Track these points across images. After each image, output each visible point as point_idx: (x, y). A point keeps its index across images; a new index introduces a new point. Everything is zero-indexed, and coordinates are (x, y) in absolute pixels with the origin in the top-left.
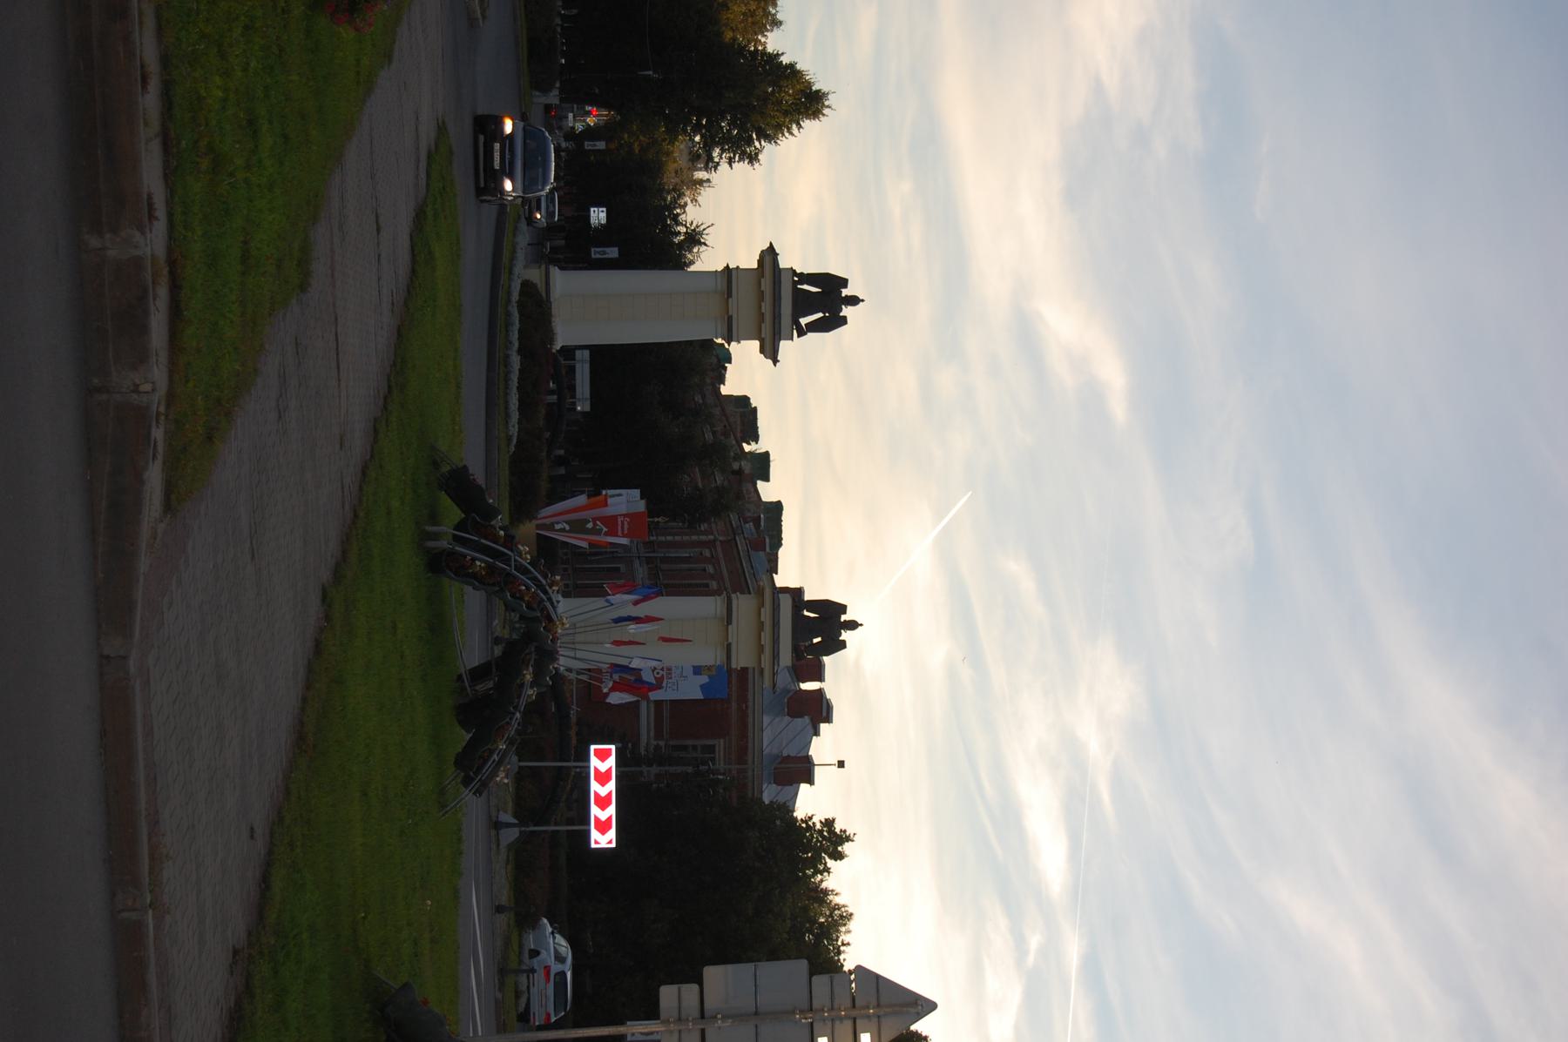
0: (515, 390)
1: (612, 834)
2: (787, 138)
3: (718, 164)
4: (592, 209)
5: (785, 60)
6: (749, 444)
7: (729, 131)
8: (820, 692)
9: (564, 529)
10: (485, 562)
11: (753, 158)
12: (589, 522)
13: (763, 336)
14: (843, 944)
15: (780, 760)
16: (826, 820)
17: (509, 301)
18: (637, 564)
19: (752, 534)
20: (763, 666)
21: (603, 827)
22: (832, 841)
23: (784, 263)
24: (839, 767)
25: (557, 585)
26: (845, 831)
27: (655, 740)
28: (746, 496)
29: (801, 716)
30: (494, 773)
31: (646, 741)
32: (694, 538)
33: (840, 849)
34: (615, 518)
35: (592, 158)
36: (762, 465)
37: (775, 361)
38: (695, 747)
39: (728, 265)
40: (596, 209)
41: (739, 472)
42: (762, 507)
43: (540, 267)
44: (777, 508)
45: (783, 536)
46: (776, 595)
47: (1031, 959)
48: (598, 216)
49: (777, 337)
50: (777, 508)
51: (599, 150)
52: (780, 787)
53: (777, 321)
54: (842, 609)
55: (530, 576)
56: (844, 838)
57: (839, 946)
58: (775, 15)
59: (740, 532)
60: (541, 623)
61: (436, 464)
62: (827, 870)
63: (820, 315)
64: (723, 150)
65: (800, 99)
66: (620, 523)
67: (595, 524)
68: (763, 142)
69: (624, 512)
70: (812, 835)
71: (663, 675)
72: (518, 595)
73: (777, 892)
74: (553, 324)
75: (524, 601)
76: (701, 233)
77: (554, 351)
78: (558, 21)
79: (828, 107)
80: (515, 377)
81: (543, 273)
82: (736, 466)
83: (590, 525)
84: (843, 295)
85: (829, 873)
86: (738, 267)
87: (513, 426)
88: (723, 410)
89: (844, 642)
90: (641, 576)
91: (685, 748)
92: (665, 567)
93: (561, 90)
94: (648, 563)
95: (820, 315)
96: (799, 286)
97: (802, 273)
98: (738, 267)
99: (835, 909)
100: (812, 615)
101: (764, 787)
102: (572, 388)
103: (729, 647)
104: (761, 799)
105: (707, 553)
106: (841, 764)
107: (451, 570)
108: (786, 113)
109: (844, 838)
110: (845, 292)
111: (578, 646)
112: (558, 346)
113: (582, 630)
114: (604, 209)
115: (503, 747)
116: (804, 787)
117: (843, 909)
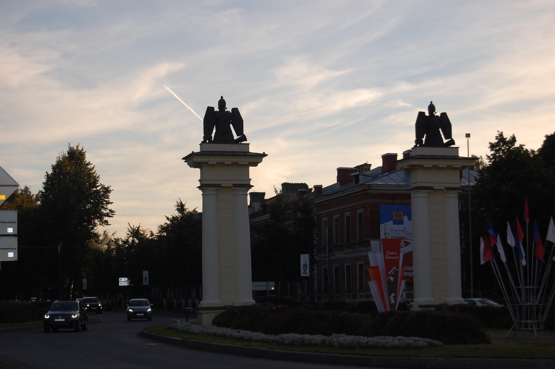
2: (95, 171)
3: (110, 210)
4: (120, 285)
5: (50, 172)
7: (91, 203)
9: (393, 296)
11: (107, 191)
12: (389, 279)
13: (247, 163)
23: (197, 149)
24: (469, 137)
34: (386, 261)
37: (264, 155)
39: (198, 187)
40: (120, 283)
42: (285, 194)
43: (200, 314)
47: (409, 105)
48: (123, 282)
51: (87, 282)
56: (501, 138)
58: (22, 190)
59: (312, 201)
65: (74, 163)
66: (390, 258)
67: (391, 275)
68: (97, 185)
71: (404, 242)
76: (133, 229)
78: (275, 296)
79: (77, 147)
80: (364, 339)
83: (392, 279)
86: (199, 180)
90: (342, 255)
97: (204, 138)
103: (448, 189)
106: (468, 135)
109: (501, 138)
110: (217, 109)
114: (120, 279)
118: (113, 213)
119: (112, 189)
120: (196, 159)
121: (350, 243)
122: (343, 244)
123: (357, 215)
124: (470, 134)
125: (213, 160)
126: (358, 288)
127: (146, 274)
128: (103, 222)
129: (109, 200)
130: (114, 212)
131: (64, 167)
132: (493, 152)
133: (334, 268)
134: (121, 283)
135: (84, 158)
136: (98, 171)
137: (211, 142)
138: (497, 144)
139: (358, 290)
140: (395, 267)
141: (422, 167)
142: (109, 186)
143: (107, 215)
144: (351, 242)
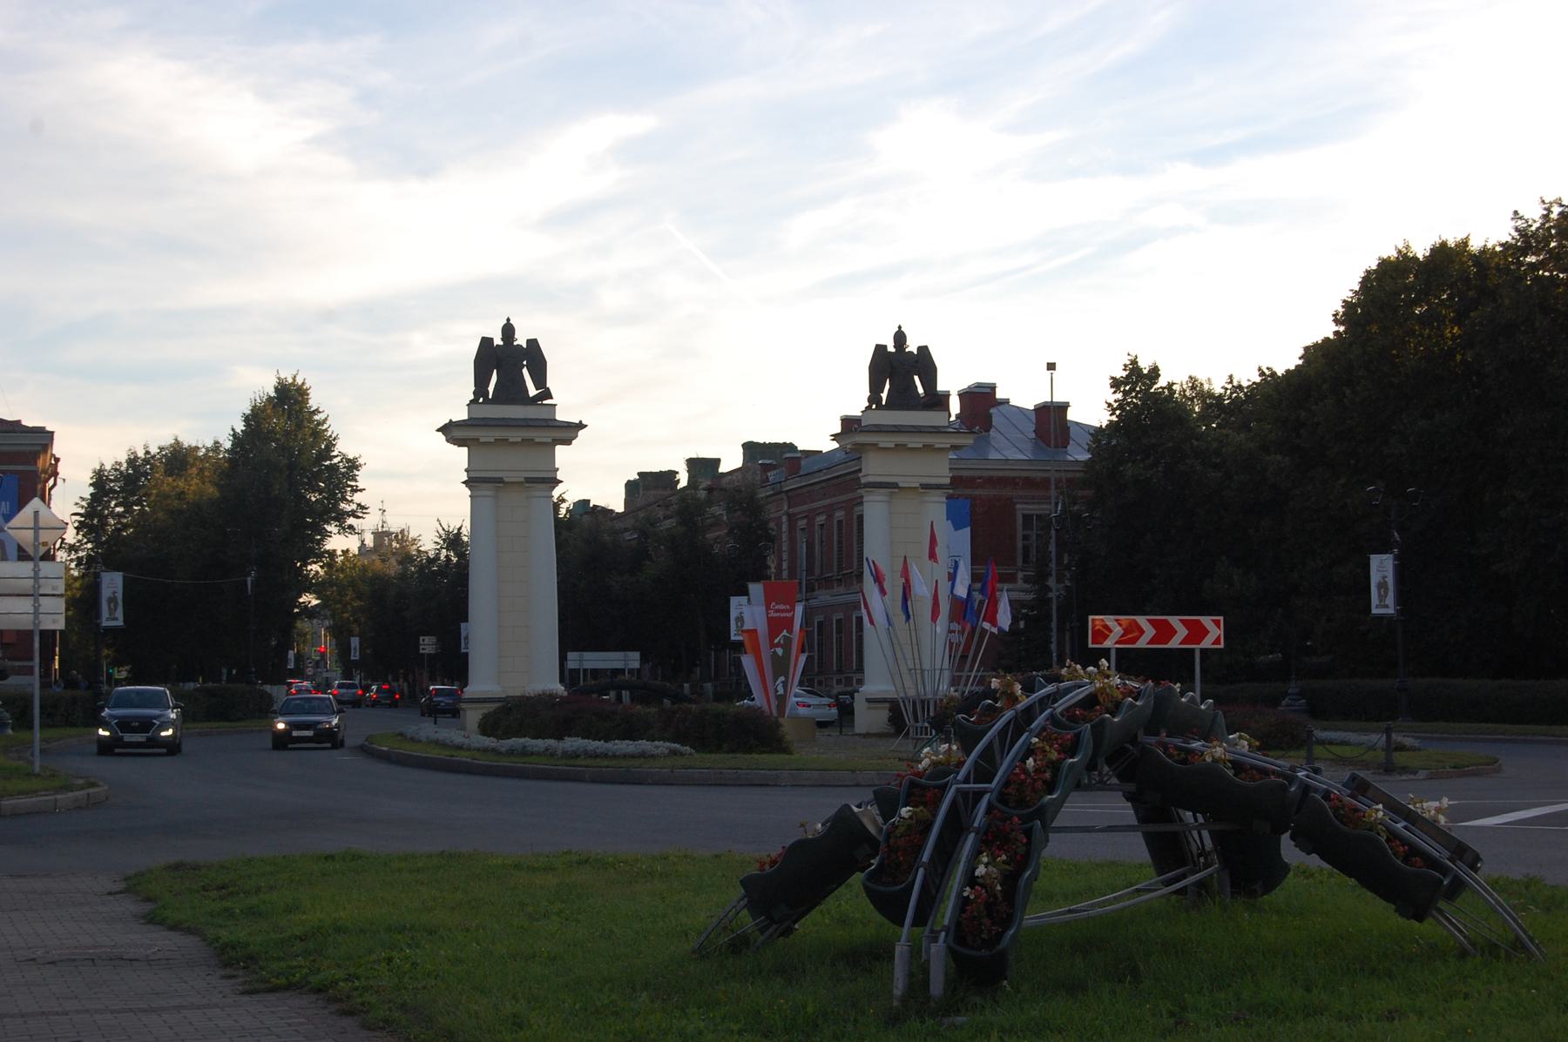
0: (609, 745)
1: (1206, 621)
3: (359, 505)
4: (421, 651)
5: (240, 427)
6: (678, 481)
8: (962, 395)
9: (783, 682)
10: (977, 853)
11: (353, 465)
12: (775, 652)
14: (1231, 382)
15: (1040, 442)
16: (1112, 387)
17: (495, 751)
18: (813, 602)
19: (782, 472)
20: (949, 446)
21: (1197, 632)
22: (1136, 380)
23: (462, 414)
24: (1054, 369)
25: (1010, 685)
26: (1125, 366)
27: (1016, 582)
28: (736, 484)
29: (990, 416)
30: (1430, 827)
31: (1017, 593)
32: (784, 537)
33: (1145, 372)
34: (771, 621)
35: (368, 651)
36: (702, 467)
37: (581, 426)
38: (1025, 538)
40: (421, 647)
41: (710, 490)
42: (749, 464)
43: (463, 709)
44: (750, 449)
45: (782, 442)
46: (863, 429)
49: (551, 423)
50: (750, 449)
52: (1071, 442)
53: (531, 423)
54: (880, 350)
55: (996, 746)
56: (1134, 368)
57: (1233, 386)
58: (207, 449)
60: (1104, 720)
61: (739, 945)
62: (1170, 386)
63: (525, 371)
64: (344, 499)
67: (778, 645)
69: (764, 608)
70: (1128, 404)
72: (1048, 775)
73: (1195, 443)
74: (532, 695)
75: (1060, 761)
76: (448, 533)
77: (566, 694)
79: (294, 379)
81: (469, 705)
82: (702, 494)
83: (780, 651)
84: (502, 343)
85: (1173, 384)
87: (657, 747)
88: (640, 509)
89: (920, 349)
90: (828, 598)
91: (1026, 550)
92: (817, 571)
93: (273, 683)
94: (813, 590)
95: (525, 371)
96: (490, 397)
98: (466, 470)
99: (1185, 395)
100: (887, 386)
101: (1070, 458)
102: (616, 672)
103: (925, 486)
104: (1085, 463)
105: (802, 523)
106: (1051, 367)
107: (1000, 936)
108: (299, 426)
109: (1134, 368)
110: (498, 341)
111: (938, 666)
112: (559, 689)
113: (917, 661)
114: (421, 638)
115: (1379, 812)
116: (1072, 415)
117: (1185, 387)
118: (364, 511)
119: (362, 463)
120: (457, 433)
121: (843, 575)
122: (830, 575)
123: (855, 517)
124: (1054, 364)
125: (486, 435)
126: (854, 664)
127: (1382, 567)
128: (344, 529)
129: (357, 484)
130: (366, 509)
131: (265, 420)
132: (1119, 396)
133: (816, 623)
134: (423, 647)
135: (308, 399)
136: (334, 427)
137: (487, 401)
138: (1126, 380)
139: (854, 668)
140: (785, 631)
141: (875, 446)
142: (357, 456)
143: (353, 514)
144: (845, 572)
